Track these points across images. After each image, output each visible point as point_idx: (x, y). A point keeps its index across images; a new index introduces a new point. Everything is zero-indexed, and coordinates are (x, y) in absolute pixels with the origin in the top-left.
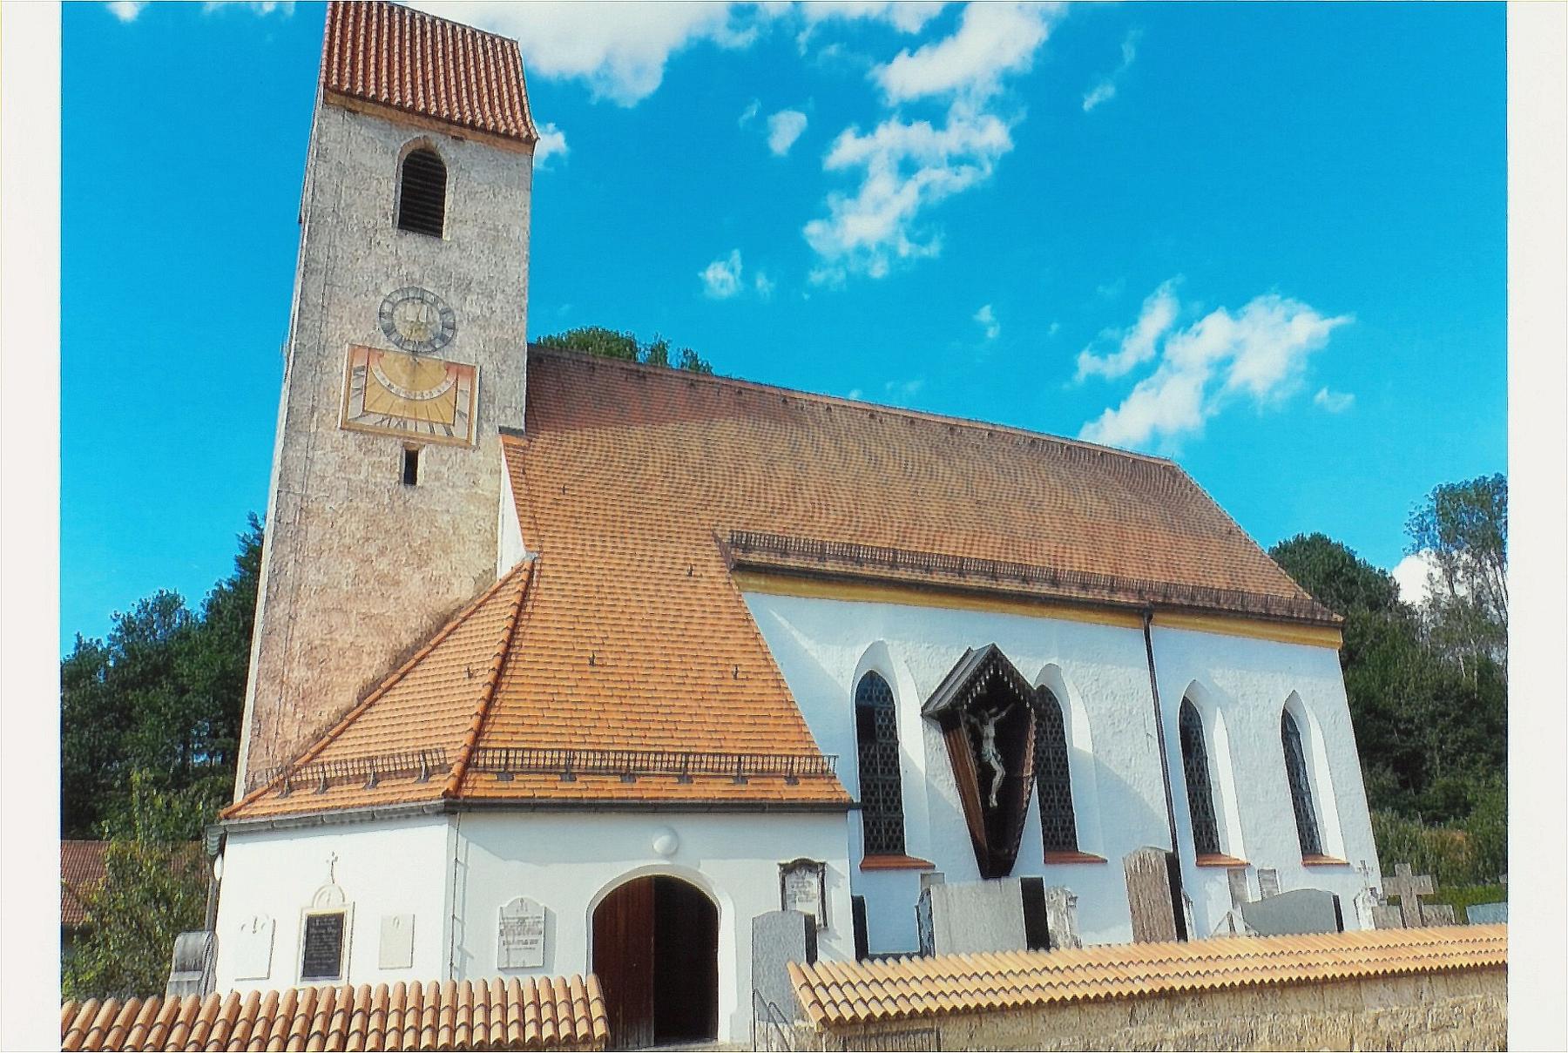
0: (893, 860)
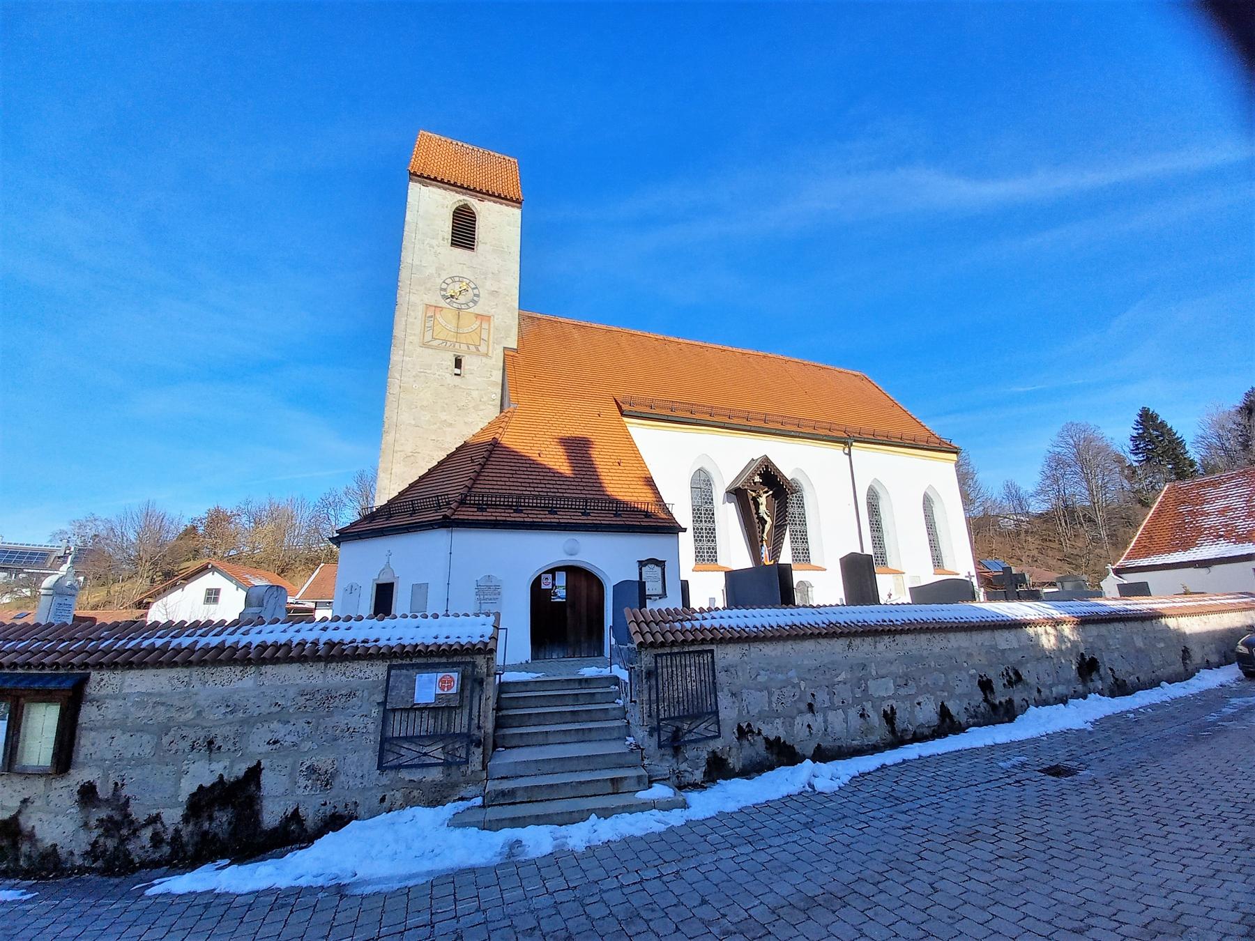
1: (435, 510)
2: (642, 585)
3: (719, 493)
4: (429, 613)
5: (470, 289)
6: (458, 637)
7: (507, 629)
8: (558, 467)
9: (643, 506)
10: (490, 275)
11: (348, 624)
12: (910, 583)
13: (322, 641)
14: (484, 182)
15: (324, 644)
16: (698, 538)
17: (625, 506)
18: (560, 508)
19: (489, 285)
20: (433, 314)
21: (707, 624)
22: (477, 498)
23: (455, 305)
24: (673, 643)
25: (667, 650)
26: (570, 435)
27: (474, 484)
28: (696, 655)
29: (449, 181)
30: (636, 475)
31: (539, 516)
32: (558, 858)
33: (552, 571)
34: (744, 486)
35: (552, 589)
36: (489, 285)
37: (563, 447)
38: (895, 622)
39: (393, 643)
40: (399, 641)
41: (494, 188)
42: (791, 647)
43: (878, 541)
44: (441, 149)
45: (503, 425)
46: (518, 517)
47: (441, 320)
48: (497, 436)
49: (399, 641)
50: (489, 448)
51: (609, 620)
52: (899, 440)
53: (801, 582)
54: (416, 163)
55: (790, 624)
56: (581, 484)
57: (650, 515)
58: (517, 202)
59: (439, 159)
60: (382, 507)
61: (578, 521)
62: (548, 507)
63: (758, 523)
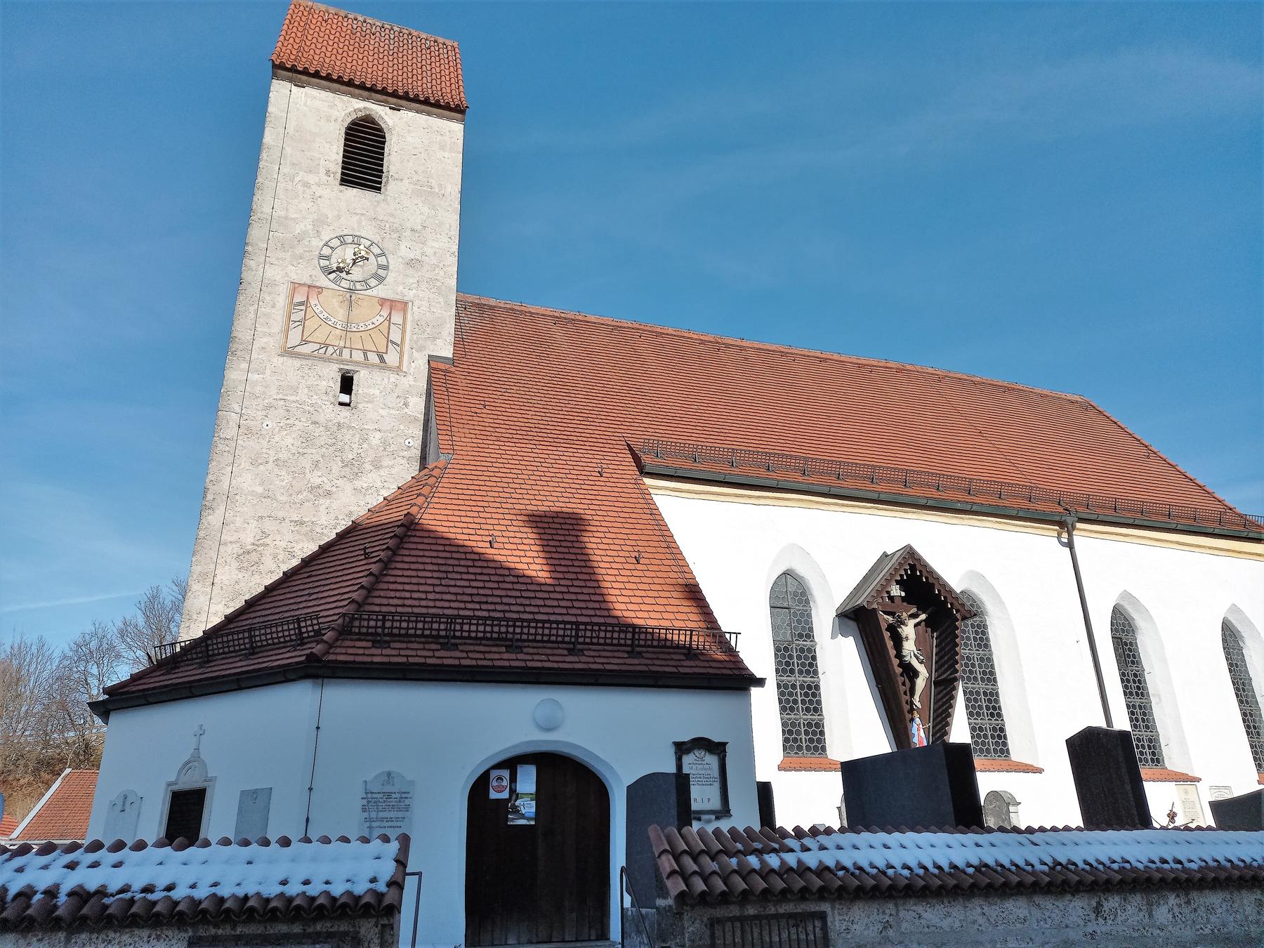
0: (814, 759)
1: (294, 646)
2: (682, 782)
3: (823, 618)
4: (273, 836)
5: (372, 257)
6: (327, 883)
7: (419, 874)
8: (525, 567)
9: (682, 638)
10: (408, 233)
11: (117, 856)
12: (1206, 794)
13: (65, 888)
14: (400, 79)
15: (70, 894)
16: (787, 704)
17: (649, 637)
18: (528, 641)
19: (405, 250)
20: (304, 299)
21: (811, 860)
22: (372, 623)
23: (344, 284)
24: (745, 896)
25: (734, 911)
26: (547, 509)
27: (367, 597)
28: (791, 922)
29: (340, 77)
30: (668, 581)
31: (488, 656)
33: (511, 764)
34: (872, 603)
35: (509, 800)
36: (405, 250)
37: (534, 530)
38: (1187, 865)
39: (202, 893)
40: (213, 890)
41: (420, 87)
42: (979, 910)
43: (1140, 708)
44: (329, 27)
45: (426, 490)
46: (449, 658)
47: (318, 309)
48: (414, 510)
49: (213, 890)
50: (398, 531)
51: (618, 857)
52: (1167, 520)
53: (994, 795)
54: (284, 49)
55: (975, 862)
56: (571, 569)
57: (696, 655)
58: (455, 110)
59: (325, 43)
60: (196, 644)
61: (562, 666)
62: (506, 639)
63: (902, 675)
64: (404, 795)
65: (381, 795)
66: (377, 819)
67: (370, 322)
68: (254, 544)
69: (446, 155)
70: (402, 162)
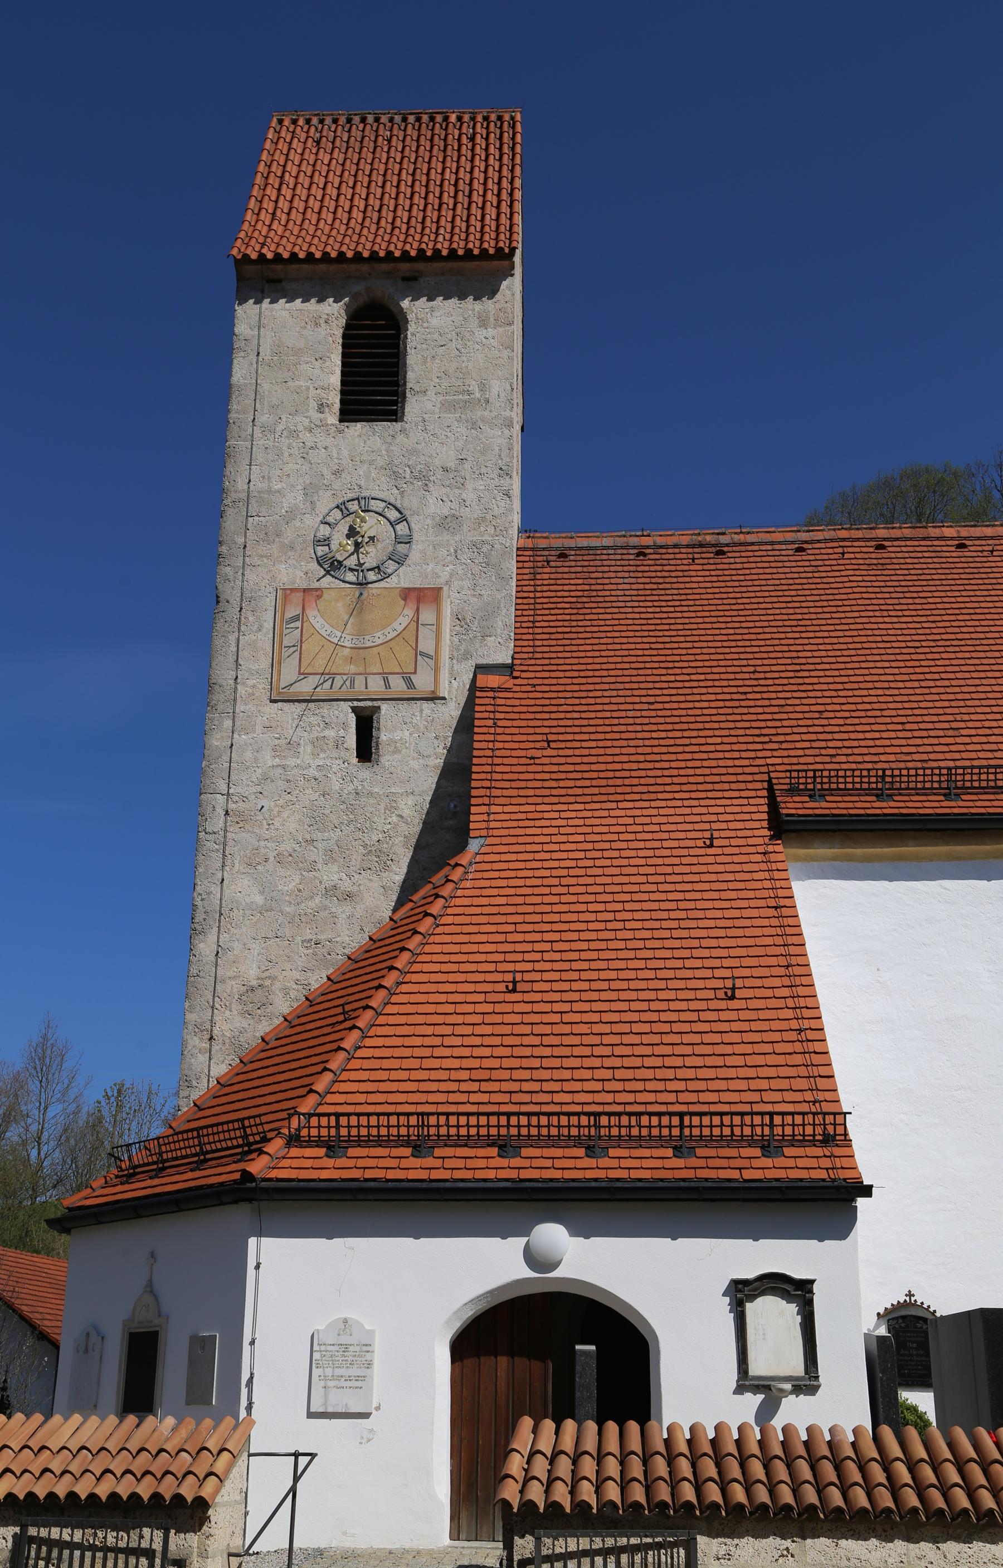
10: (440, 473)
20: (299, 611)
32: (47, 1525)
64: (365, 1348)
65: (337, 1348)
66: (334, 1378)
67: (389, 629)
68: (258, 979)
69: (491, 332)
70: (425, 362)
